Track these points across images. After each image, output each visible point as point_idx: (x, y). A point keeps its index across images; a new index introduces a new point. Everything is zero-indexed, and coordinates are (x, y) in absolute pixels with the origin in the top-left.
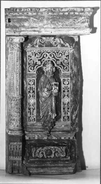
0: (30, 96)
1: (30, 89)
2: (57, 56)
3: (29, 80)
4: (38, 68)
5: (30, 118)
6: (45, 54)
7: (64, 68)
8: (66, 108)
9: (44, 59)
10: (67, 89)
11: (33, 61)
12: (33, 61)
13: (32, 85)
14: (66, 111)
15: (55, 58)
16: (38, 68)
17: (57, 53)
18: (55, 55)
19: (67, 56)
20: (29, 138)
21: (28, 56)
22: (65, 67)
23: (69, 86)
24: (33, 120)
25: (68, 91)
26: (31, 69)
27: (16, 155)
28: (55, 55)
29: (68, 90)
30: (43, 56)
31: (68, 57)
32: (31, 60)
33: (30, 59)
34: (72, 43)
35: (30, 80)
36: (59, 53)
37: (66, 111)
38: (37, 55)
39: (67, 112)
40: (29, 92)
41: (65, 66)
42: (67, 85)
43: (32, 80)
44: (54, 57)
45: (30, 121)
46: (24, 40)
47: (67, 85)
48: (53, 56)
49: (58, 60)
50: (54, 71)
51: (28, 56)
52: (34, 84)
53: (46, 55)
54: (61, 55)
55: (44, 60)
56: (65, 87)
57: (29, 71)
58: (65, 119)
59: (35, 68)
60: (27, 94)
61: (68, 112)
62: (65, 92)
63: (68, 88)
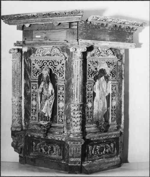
0: (33, 99)
2: (54, 64)
3: (32, 84)
4: (39, 74)
5: (88, 121)
6: (44, 63)
10: (62, 94)
12: (36, 68)
13: (62, 90)
14: (34, 112)
16: (39, 74)
17: (54, 62)
18: (53, 64)
19: (62, 65)
20: (31, 136)
21: (87, 65)
22: (114, 76)
24: (90, 122)
25: (63, 97)
26: (34, 75)
28: (53, 64)
30: (44, 64)
35: (33, 84)
38: (94, 64)
39: (61, 115)
40: (88, 97)
41: (113, 74)
43: (35, 84)
44: (52, 65)
45: (59, 123)
46: (86, 49)
52: (63, 90)
53: (45, 63)
55: (44, 67)
56: (60, 92)
57: (33, 77)
60: (86, 99)
61: (62, 116)
63: (63, 94)
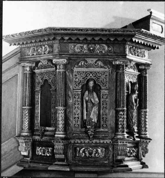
1: (76, 101)
2: (98, 75)
4: (95, 79)
6: (88, 74)
7: (104, 86)
8: (105, 104)
9: (44, 78)
11: (79, 80)
15: (96, 77)
16: (95, 79)
18: (96, 75)
23: (107, 100)
27: (122, 41)
28: (96, 75)
29: (107, 103)
31: (106, 76)
32: (77, 78)
33: (76, 77)
34: (91, 95)
36: (99, 73)
37: (105, 120)
42: (106, 98)
45: (75, 127)
47: (106, 98)
48: (94, 75)
49: (81, 81)
50: (113, 63)
51: (74, 75)
52: (79, 98)
53: (88, 74)
54: (101, 74)
58: (104, 127)
59: (80, 84)
62: (104, 104)
